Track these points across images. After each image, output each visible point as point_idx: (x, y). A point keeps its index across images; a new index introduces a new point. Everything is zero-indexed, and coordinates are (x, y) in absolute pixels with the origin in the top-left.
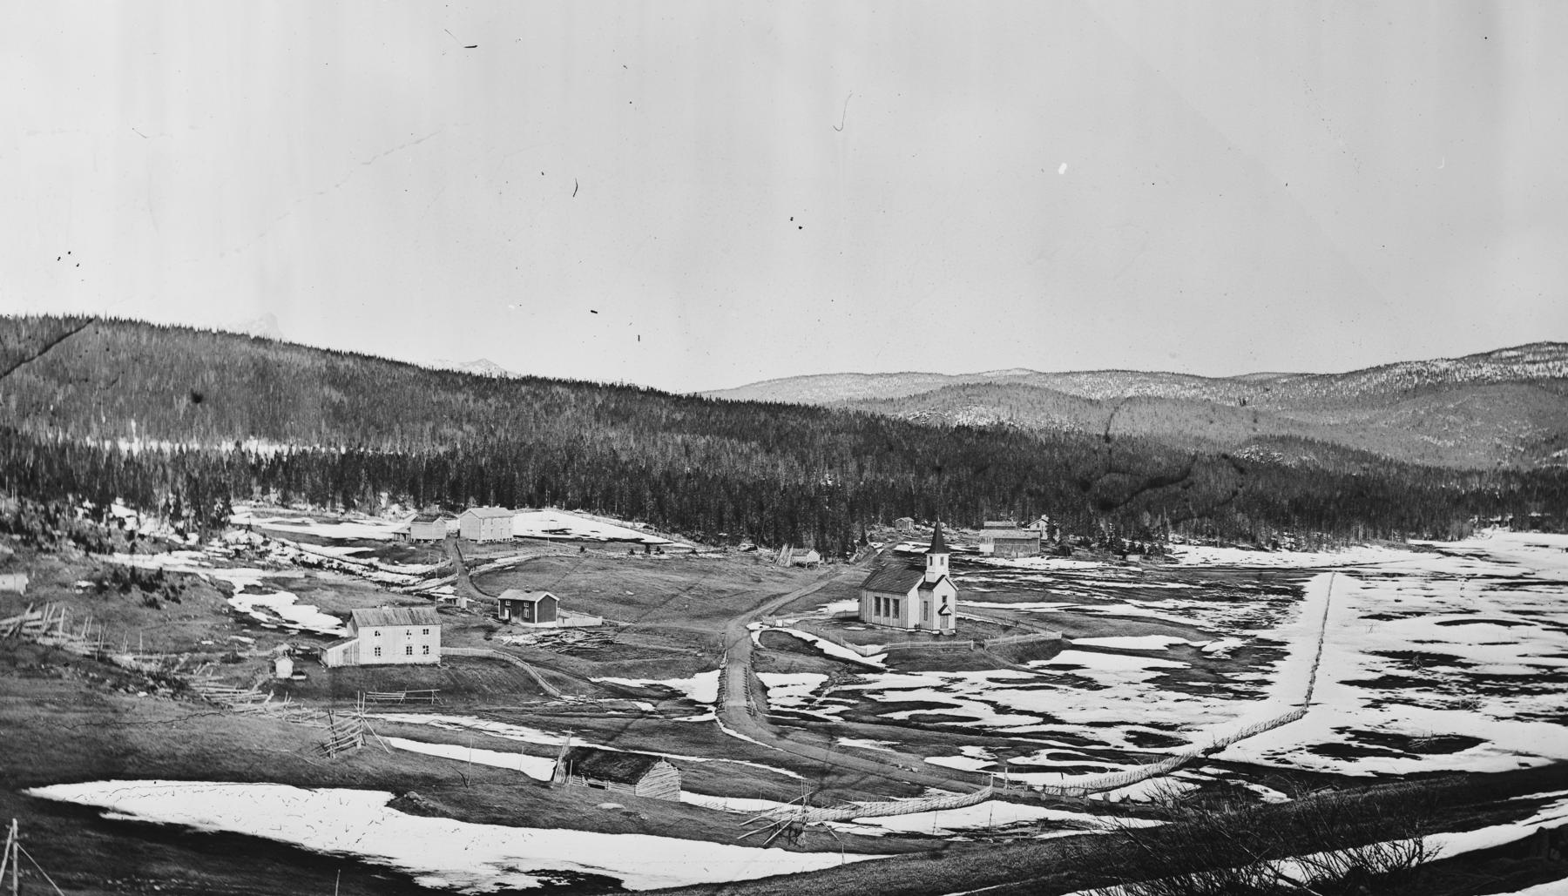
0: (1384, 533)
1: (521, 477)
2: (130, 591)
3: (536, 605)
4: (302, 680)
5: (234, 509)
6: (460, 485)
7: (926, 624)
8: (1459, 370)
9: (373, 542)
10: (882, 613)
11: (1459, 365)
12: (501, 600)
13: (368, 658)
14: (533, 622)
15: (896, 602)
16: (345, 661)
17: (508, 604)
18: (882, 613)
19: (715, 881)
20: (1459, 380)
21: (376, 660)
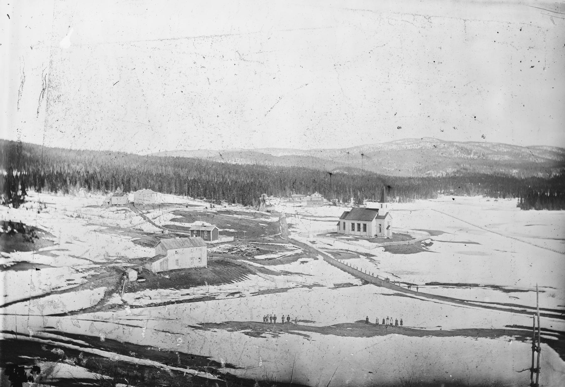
3: (211, 232)
4: (144, 282)
7: (379, 234)
8: (386, 147)
13: (172, 266)
14: (210, 240)
16: (161, 268)
18: (362, 229)
19: (461, 328)
20: (386, 150)
21: (176, 267)
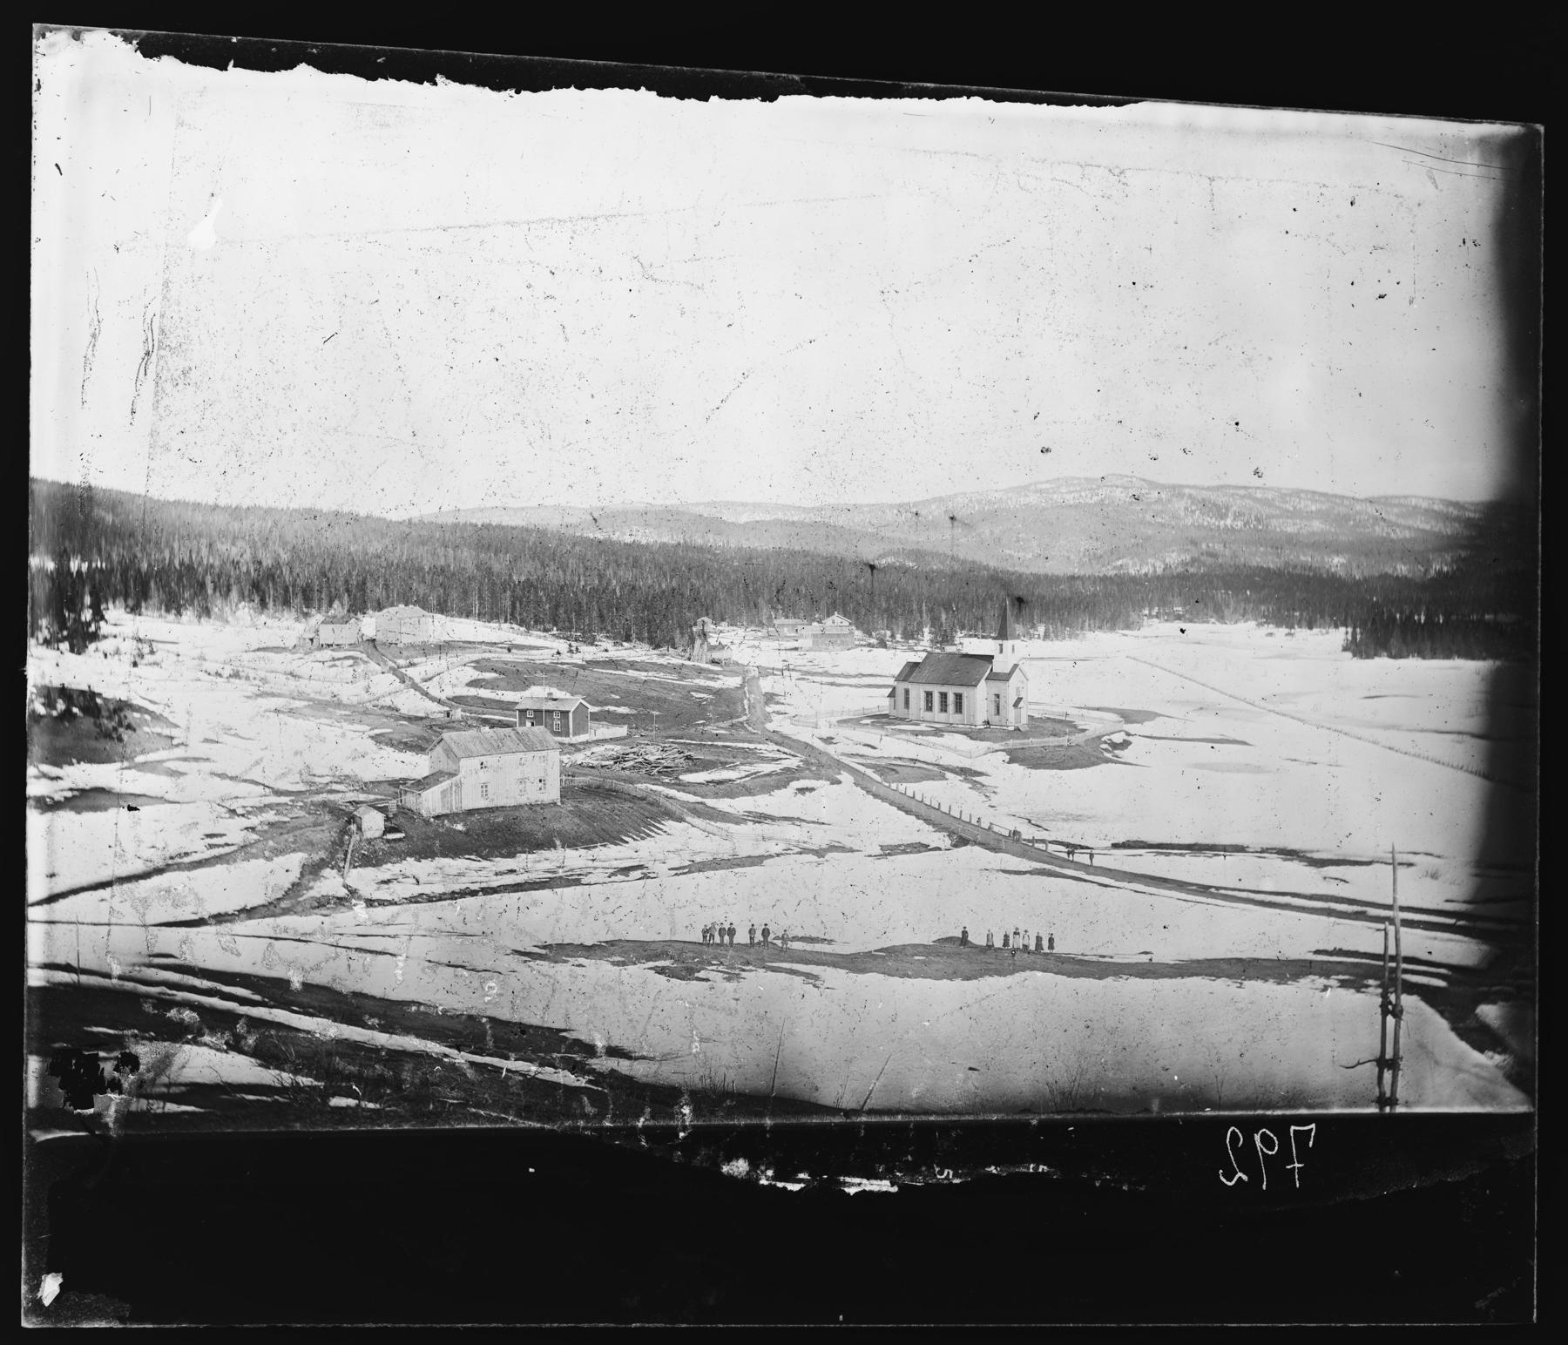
0: (794, 613)
1: (1237, 516)
2: (304, 984)
3: (571, 715)
4: (400, 840)
5: (107, 615)
6: (312, 590)
7: (995, 719)
9: (1049, 725)
10: (951, 708)
11: (1010, 495)
12: (520, 711)
13: (472, 800)
14: (567, 735)
15: (959, 697)
16: (443, 806)
17: (530, 715)
18: (951, 708)
21: (482, 804)
